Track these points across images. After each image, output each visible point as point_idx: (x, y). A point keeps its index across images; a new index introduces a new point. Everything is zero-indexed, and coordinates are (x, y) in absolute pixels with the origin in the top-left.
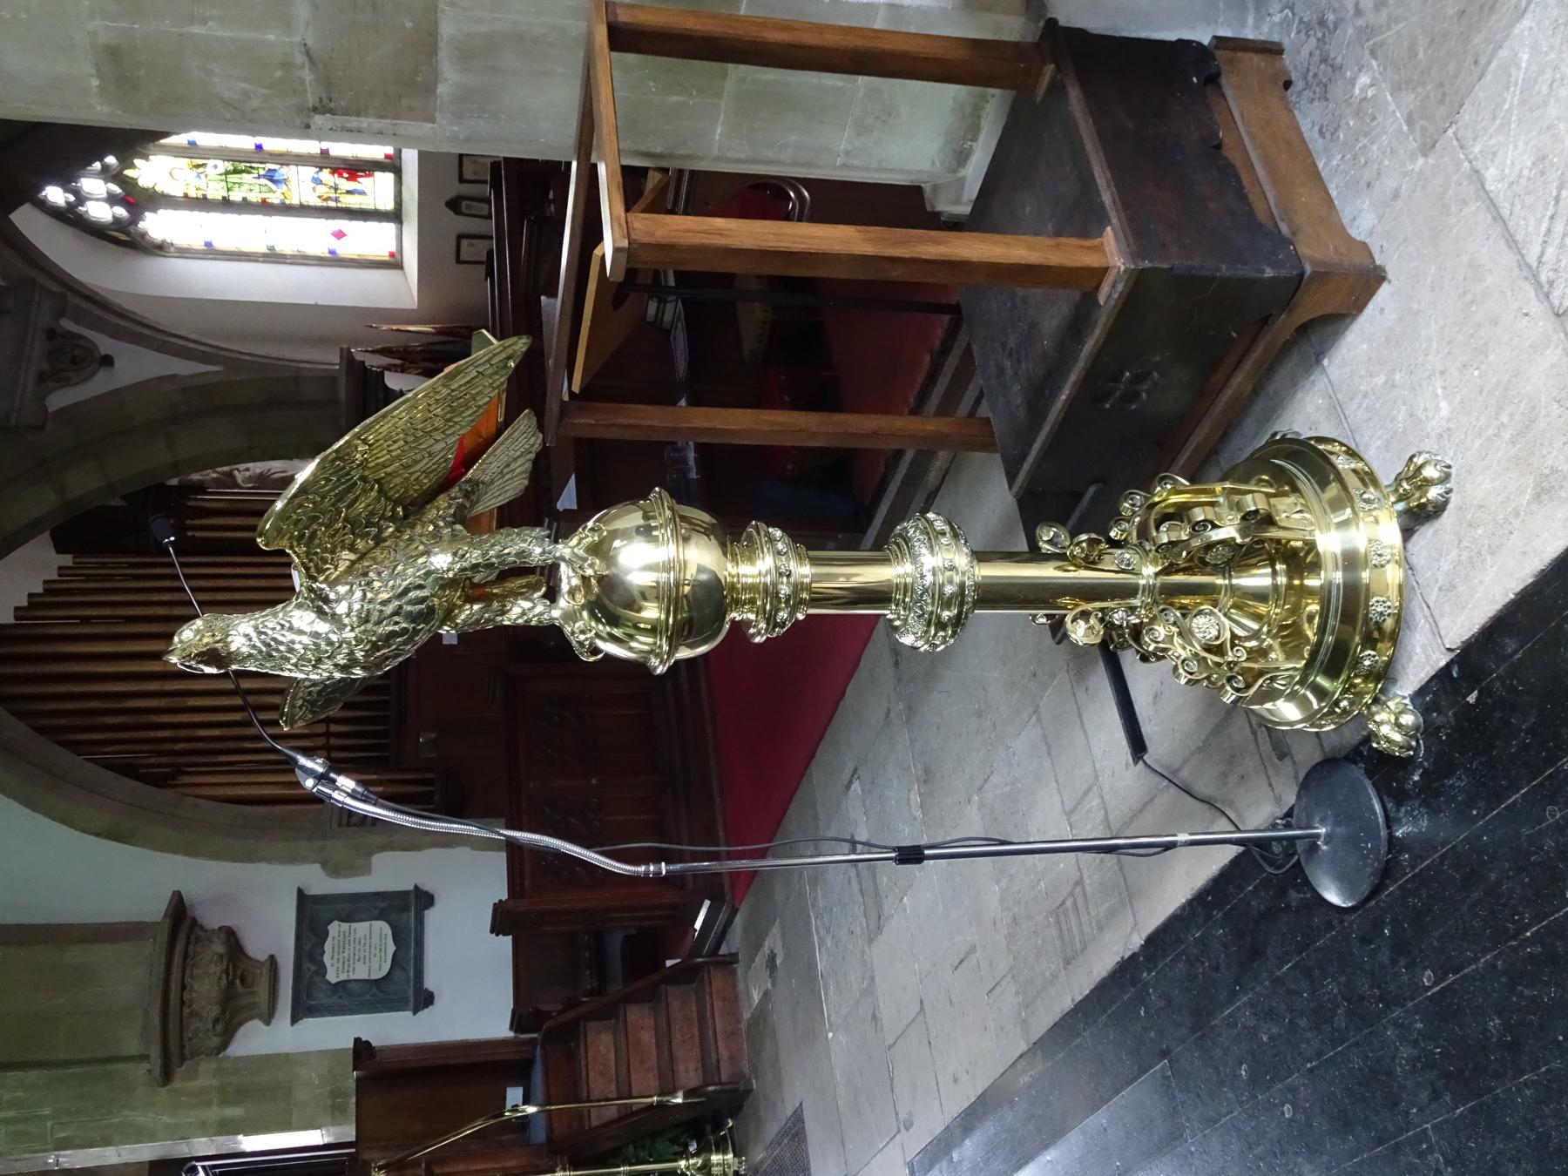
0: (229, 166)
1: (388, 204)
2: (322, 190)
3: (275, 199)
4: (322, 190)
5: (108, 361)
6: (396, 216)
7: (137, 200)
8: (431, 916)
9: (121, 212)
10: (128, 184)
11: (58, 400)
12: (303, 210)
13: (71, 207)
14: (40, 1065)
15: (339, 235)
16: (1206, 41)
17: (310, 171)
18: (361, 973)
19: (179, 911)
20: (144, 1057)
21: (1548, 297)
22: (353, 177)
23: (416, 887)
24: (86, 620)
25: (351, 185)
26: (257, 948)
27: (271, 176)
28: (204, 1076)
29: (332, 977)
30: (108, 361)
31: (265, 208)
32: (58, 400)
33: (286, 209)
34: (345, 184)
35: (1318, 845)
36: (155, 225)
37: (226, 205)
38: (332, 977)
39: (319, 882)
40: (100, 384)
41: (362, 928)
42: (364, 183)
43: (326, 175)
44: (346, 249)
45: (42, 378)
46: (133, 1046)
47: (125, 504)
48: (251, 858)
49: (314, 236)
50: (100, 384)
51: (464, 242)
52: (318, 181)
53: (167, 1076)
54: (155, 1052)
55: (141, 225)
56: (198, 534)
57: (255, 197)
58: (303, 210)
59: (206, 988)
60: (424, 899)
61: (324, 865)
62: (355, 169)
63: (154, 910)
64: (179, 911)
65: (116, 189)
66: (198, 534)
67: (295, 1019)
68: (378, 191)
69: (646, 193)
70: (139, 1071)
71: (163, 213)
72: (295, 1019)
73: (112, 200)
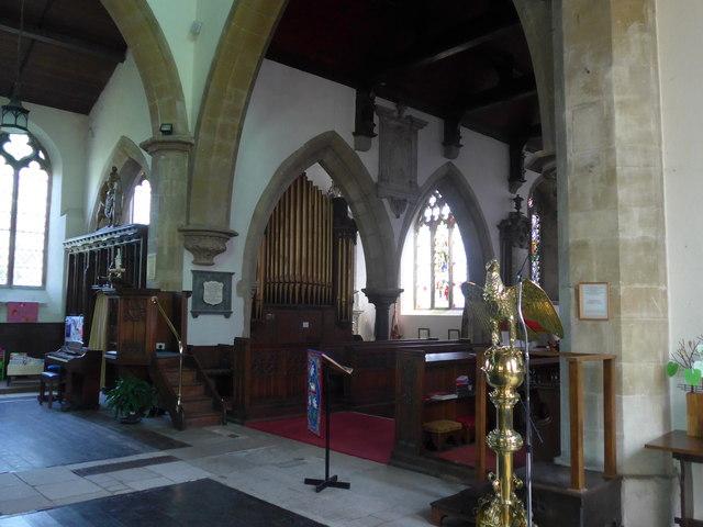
3: (436, 268)
5: (398, 217)
7: (433, 225)
8: (222, 317)
9: (428, 220)
11: (385, 201)
12: (433, 277)
13: (429, 205)
14: (189, 193)
15: (425, 289)
17: (447, 279)
18: (206, 293)
19: (234, 234)
20: (188, 224)
23: (403, 290)
24: (313, 207)
25: (443, 293)
26: (217, 259)
28: (178, 243)
29: (206, 284)
30: (398, 217)
31: (433, 265)
32: (385, 201)
33: (433, 272)
34: (443, 291)
36: (425, 229)
37: (433, 252)
38: (206, 284)
39: (236, 280)
40: (390, 213)
41: (220, 294)
42: (444, 297)
43: (446, 284)
44: (420, 290)
45: (392, 198)
46: (193, 220)
48: (245, 257)
49: (425, 280)
50: (390, 213)
53: (179, 231)
54: (190, 227)
55: (424, 226)
57: (436, 261)
58: (433, 277)
59: (209, 244)
60: (228, 315)
61: (241, 281)
62: (449, 294)
63: (233, 227)
64: (234, 234)
65: (436, 219)
67: (193, 272)
68: (442, 302)
69: (202, 475)
70: (182, 222)
71: (429, 233)
72: (193, 272)
73: (432, 217)
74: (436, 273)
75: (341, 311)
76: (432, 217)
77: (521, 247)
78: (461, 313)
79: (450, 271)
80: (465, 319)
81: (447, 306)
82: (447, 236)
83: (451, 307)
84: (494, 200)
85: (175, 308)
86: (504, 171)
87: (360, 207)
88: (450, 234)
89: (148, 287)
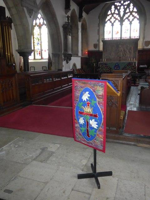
0: (39, 38)
1: (36, 58)
2: (37, 50)
4: (37, 50)
5: (30, 17)
6: (35, 59)
9: (38, 24)
10: (42, 25)
11: (25, 8)
13: (38, 18)
16: (137, 14)
17: (40, 48)
21: (72, 190)
22: (39, 54)
27: (38, 44)
34: (38, 53)
35: (84, 61)
42: (39, 55)
43: (39, 50)
45: (28, 7)
47: (122, 17)
51: (34, 68)
52: (38, 49)
56: (4, 28)
66: (4, 28)
73: (40, 23)
74: (35, 46)
75: (8, 60)
76: (40, 23)
77: (70, 35)
78: (47, 60)
79: (41, 45)
80: (50, 62)
81: (40, 58)
82: (39, 31)
83: (42, 58)
84: (62, 17)
85: (99, 68)
86: (64, 6)
87: (14, 11)
88: (40, 30)
89: (132, 87)
